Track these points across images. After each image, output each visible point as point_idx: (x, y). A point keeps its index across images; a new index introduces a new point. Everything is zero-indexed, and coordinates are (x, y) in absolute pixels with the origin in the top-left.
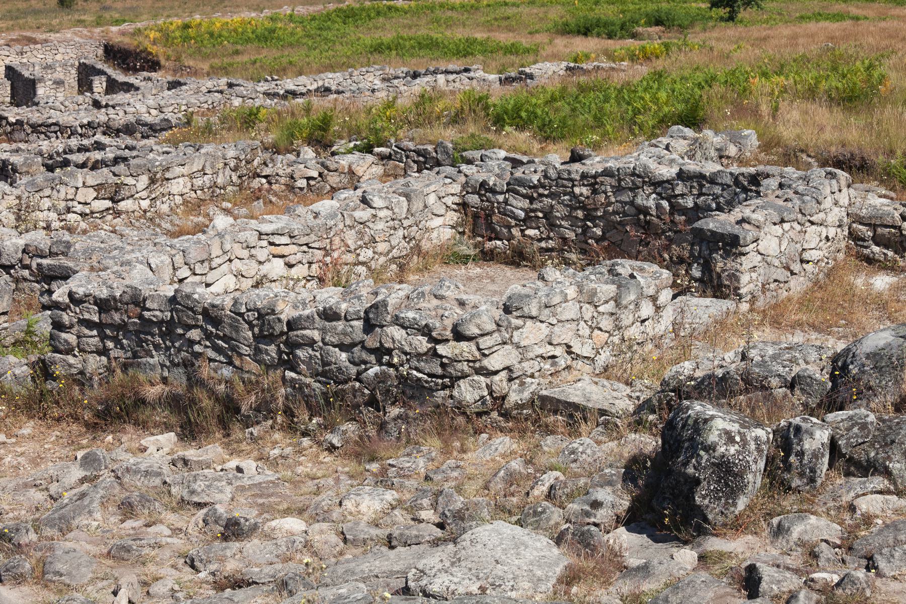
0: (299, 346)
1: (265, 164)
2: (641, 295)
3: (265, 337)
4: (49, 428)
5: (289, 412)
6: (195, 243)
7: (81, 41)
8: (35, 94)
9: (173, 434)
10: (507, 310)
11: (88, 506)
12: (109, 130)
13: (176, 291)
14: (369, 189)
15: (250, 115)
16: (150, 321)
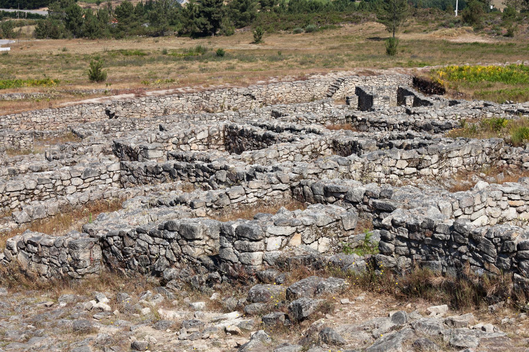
0: (523, 259)
1: (506, 152)
3: (504, 253)
4: (374, 297)
5: (514, 298)
6: (466, 196)
7: (400, 75)
8: (372, 104)
9: (446, 305)
11: (395, 343)
12: (416, 127)
13: (454, 223)
15: (498, 123)
16: (438, 239)
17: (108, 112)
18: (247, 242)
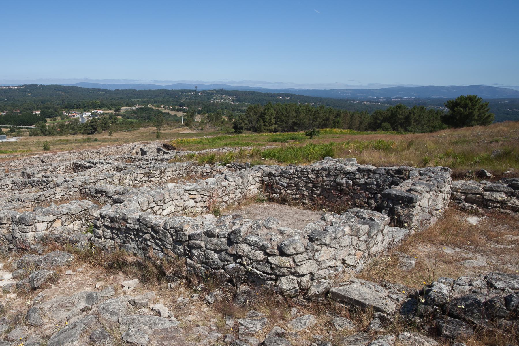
0: (194, 248)
2: (378, 231)
3: (178, 241)
9: (136, 280)
10: (311, 240)
14: (227, 174)
16: (129, 228)
17: (42, 161)
18: (24, 227)
